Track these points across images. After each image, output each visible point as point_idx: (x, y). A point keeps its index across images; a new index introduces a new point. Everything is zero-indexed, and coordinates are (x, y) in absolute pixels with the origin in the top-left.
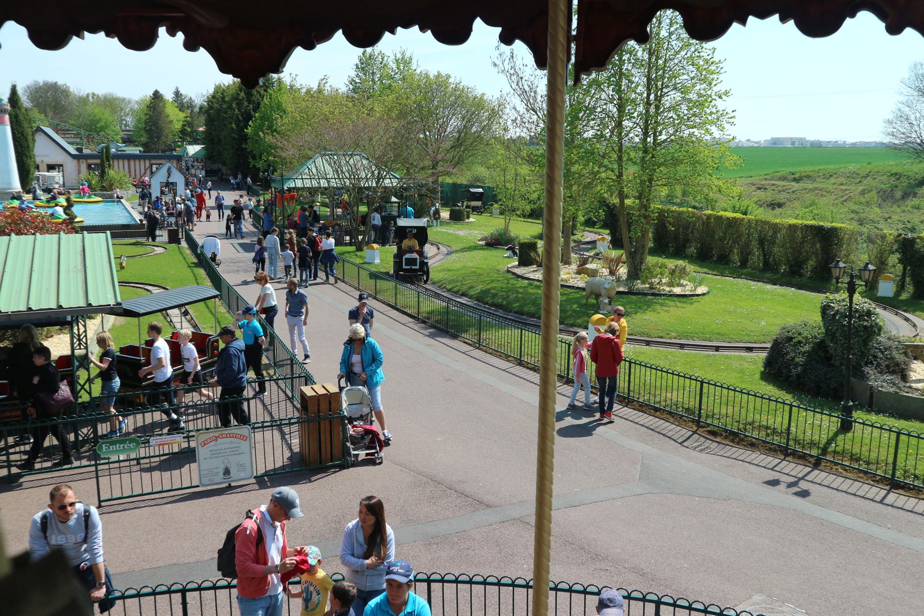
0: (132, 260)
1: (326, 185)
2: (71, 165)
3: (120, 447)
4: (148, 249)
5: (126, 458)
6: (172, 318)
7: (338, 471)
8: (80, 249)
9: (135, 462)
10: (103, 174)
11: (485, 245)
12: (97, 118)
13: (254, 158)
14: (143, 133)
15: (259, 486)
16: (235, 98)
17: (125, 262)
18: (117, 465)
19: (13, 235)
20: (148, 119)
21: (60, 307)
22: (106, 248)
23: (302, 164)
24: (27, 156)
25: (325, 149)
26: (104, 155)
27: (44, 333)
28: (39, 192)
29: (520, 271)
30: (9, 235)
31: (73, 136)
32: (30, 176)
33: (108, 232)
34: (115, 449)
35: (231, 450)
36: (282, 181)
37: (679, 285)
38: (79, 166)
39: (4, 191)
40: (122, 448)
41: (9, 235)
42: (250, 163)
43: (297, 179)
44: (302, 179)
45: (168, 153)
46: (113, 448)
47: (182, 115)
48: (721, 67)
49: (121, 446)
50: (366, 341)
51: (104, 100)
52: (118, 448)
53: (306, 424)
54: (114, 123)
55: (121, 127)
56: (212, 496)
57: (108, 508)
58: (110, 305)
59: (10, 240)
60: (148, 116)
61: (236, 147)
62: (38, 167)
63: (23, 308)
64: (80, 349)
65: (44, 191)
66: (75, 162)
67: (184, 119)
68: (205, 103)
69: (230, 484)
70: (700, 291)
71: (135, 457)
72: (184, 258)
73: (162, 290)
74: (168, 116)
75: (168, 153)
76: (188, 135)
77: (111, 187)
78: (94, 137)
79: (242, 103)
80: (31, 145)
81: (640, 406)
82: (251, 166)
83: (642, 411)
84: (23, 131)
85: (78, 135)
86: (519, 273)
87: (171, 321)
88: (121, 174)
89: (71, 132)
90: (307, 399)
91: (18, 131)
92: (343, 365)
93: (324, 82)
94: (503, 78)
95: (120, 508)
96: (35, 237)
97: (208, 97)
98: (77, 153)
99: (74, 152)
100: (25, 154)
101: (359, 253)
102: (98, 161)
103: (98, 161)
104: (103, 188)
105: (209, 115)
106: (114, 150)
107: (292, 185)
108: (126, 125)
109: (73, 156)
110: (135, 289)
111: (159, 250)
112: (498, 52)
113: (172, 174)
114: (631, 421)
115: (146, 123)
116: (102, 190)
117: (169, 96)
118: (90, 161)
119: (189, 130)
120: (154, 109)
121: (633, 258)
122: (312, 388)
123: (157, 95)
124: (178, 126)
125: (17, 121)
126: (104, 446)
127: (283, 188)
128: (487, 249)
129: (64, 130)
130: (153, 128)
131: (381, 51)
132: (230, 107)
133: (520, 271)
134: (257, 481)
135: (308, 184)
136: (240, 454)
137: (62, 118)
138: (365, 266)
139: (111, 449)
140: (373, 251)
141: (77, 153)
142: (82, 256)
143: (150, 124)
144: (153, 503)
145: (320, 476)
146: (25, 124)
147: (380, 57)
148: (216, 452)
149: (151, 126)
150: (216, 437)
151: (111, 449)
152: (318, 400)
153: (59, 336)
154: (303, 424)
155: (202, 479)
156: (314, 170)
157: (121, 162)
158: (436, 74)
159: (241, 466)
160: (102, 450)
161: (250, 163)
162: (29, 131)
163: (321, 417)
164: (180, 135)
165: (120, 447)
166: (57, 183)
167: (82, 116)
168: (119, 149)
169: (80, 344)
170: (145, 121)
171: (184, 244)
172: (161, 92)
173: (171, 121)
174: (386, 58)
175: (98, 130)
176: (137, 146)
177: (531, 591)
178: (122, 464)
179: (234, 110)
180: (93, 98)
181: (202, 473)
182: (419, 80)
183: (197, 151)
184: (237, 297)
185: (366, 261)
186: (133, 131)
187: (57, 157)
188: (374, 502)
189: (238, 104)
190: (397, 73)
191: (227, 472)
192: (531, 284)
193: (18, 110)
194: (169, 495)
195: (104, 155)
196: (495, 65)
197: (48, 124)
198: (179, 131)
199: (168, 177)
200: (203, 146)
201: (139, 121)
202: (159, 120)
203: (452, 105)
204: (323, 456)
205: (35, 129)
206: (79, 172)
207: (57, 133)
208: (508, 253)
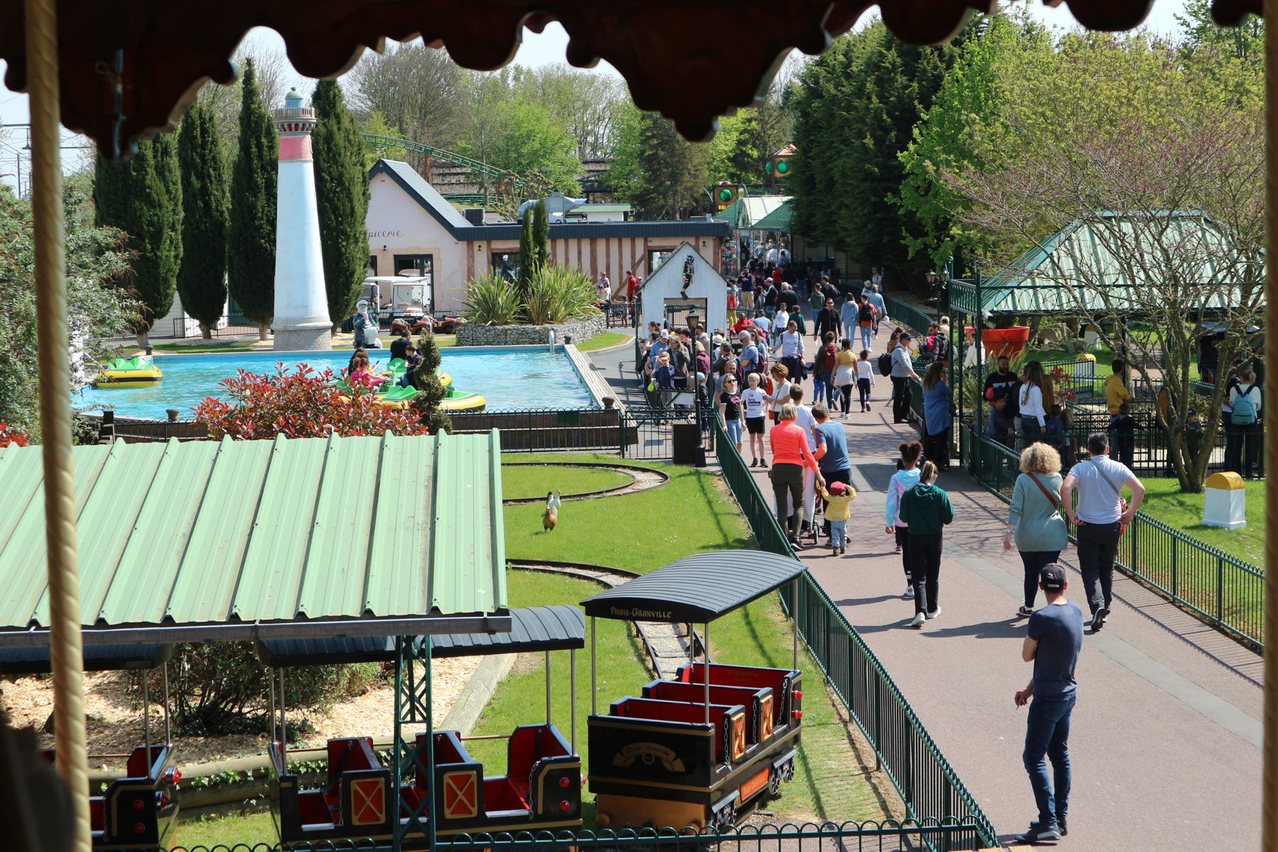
1: (1100, 304)
2: (450, 255)
4: (620, 477)
6: (657, 659)
8: (426, 472)
10: (523, 284)
12: (524, 131)
16: (874, 65)
19: (281, 436)
20: (648, 129)
21: (368, 613)
22: (375, 471)
23: (1036, 248)
24: (348, 238)
26: (531, 230)
27: (344, 682)
30: (219, 438)
31: (462, 179)
32: (354, 286)
33: (496, 432)
38: (471, 257)
39: (290, 326)
41: (219, 438)
43: (1019, 287)
44: (1034, 287)
48: (309, 366)
51: (543, 85)
54: (566, 142)
58: (481, 614)
59: (219, 449)
61: (873, 199)
62: (373, 263)
63: (287, 613)
64: (413, 720)
65: (384, 323)
67: (742, 127)
68: (798, 82)
72: (709, 503)
73: (628, 580)
79: (893, 80)
80: (359, 210)
84: (341, 174)
87: (655, 668)
89: (458, 170)
91: (330, 174)
96: (329, 442)
98: (466, 224)
99: (460, 222)
100: (344, 233)
101: (1189, 499)
102: (515, 245)
103: (515, 245)
104: (524, 316)
105: (805, 115)
107: (1006, 306)
108: (595, 148)
109: (458, 234)
110: (575, 580)
111: (647, 481)
113: (695, 277)
116: (521, 321)
118: (498, 245)
125: (330, 150)
130: (662, 153)
132: (860, 92)
135: (1049, 301)
138: (1196, 536)
140: (1224, 492)
141: (466, 224)
146: (348, 158)
149: (656, 147)
153: (381, 693)
156: (1067, 264)
157: (573, 244)
162: (356, 173)
164: (732, 170)
166: (416, 303)
169: (412, 711)
170: (641, 134)
176: (618, 200)
179: (869, 98)
180: (516, 79)
183: (770, 210)
185: (1206, 520)
187: (421, 237)
189: (880, 82)
193: (333, 122)
195: (531, 230)
197: (404, 152)
198: (729, 158)
199: (686, 286)
206: (470, 273)
207: (425, 175)
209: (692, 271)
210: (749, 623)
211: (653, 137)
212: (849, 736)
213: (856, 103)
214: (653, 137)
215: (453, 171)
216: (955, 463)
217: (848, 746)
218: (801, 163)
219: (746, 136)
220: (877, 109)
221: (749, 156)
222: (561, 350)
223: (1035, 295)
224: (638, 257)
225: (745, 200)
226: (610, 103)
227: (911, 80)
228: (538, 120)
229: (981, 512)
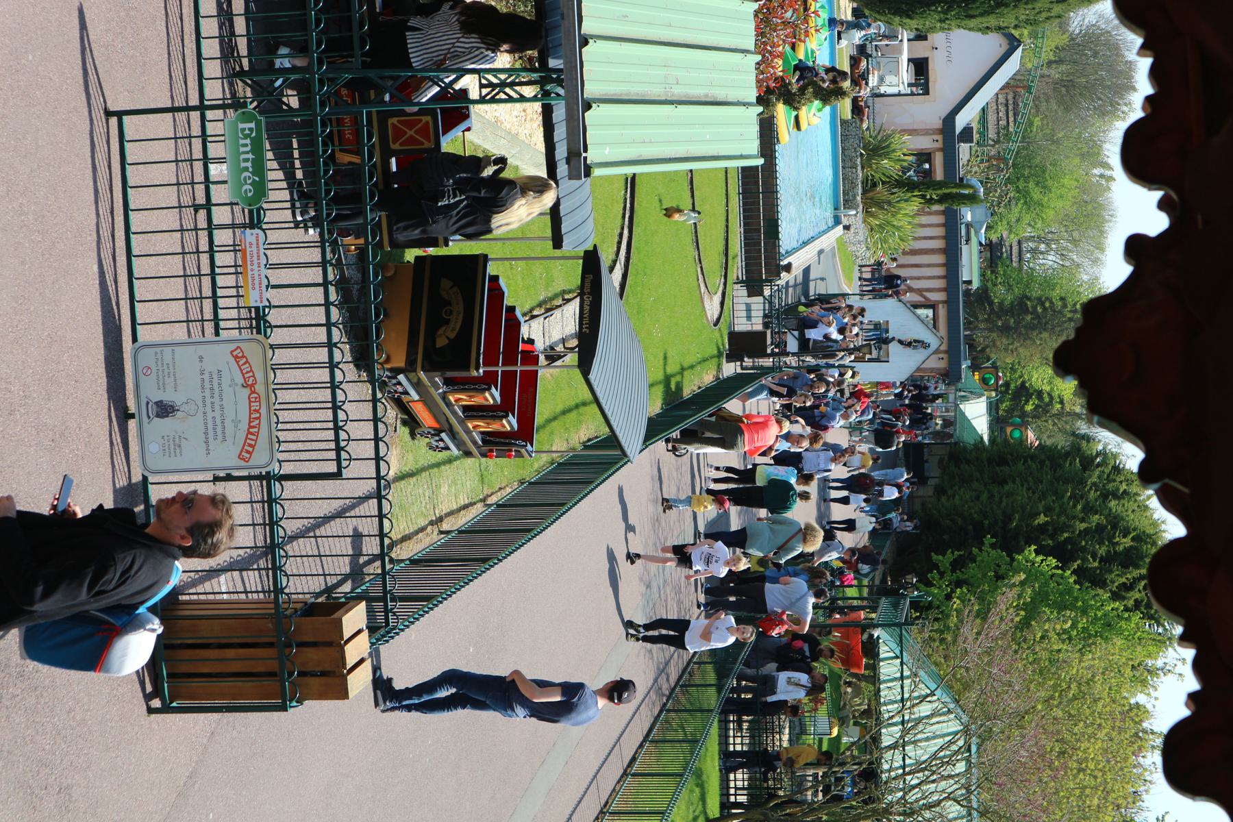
0: (688, 239)
1: (886, 741)
2: (929, 112)
3: (246, 160)
4: (716, 281)
6: (541, 319)
7: (143, 689)
8: (721, 95)
13: (957, 565)
15: (121, 489)
17: (683, 218)
21: (585, 42)
23: (940, 679)
24: (945, 13)
25: (983, 741)
28: (857, 36)
31: (1003, 123)
32: (897, 19)
33: (760, 162)
34: (242, 149)
35: (218, 422)
36: (895, 625)
38: (926, 132)
40: (243, 165)
42: (944, 555)
43: (902, 663)
44: (902, 678)
45: (964, 348)
46: (246, 145)
49: (249, 164)
53: (273, 611)
55: (1031, 238)
56: (107, 372)
57: (103, 131)
58: (586, 150)
61: (987, 522)
62: (920, 37)
66: (938, 124)
68: (1100, 447)
69: (132, 416)
75: (964, 348)
77: (872, 204)
78: (999, 170)
79: (1101, 543)
80: (972, 23)
82: (934, 556)
85: (1004, 135)
87: (533, 317)
89: (1011, 119)
90: (336, 615)
95: (101, 157)
97: (1115, 456)
98: (958, 129)
99: (961, 121)
102: (939, 175)
103: (939, 175)
104: (870, 185)
106: (969, 217)
107: (884, 652)
108: (1034, 251)
109: (949, 120)
110: (616, 239)
111: (712, 307)
113: (909, 351)
115: (1041, 301)
116: (865, 182)
118: (938, 159)
119: (1029, 408)
122: (359, 632)
126: (252, 125)
129: (1016, 104)
132: (1089, 509)
134: (136, 484)
135: (889, 692)
136: (207, 442)
137: (1047, 101)
139: (242, 142)
141: (958, 129)
142: (703, 99)
144: (105, 233)
148: (216, 386)
149: (1034, 312)
150: (252, 385)
151: (242, 142)
152: (329, 644)
155: (152, 350)
157: (940, 231)
159: (175, 445)
161: (944, 555)
162: (1008, 19)
163: (287, 651)
164: (1012, 386)
165: (246, 160)
166: (881, 79)
167: (1054, 148)
168: (972, 231)
171: (730, 369)
175: (1021, 184)
176: (983, 275)
177: (236, 208)
179: (1083, 520)
180: (1102, 176)
181: (168, 350)
183: (974, 423)
186: (1020, 269)
189: (1100, 528)
191: (164, 410)
194: (119, 271)
195: (954, 191)
197: (1029, 66)
198: (1023, 383)
199: (900, 342)
200: (986, 438)
201: (1048, 283)
205: (1016, 33)
209: (915, 348)
211: (1045, 309)
212: (472, 504)
214: (1045, 309)
215: (1011, 114)
219: (1047, 400)
221: (1027, 402)
222: (837, 221)
223: (895, 679)
225: (984, 398)
228: (1061, 197)
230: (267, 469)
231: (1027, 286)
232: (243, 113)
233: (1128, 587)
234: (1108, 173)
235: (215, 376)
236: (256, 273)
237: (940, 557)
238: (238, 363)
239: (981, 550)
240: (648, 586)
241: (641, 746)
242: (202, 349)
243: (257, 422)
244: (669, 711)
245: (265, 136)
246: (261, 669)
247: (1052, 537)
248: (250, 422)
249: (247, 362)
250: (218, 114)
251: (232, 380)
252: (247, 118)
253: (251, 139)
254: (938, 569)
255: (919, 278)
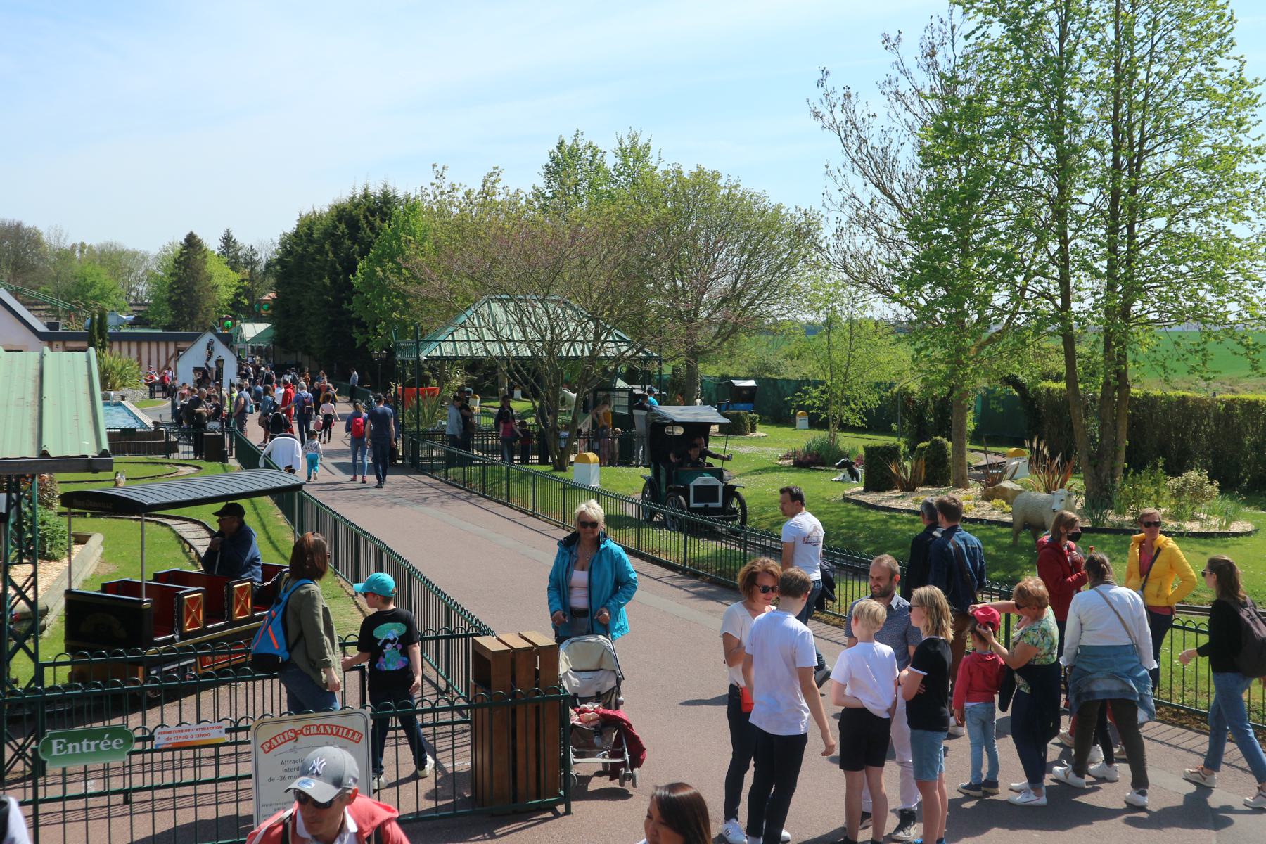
3: (89, 746)
4: (168, 469)
5: (102, 790)
9: (120, 798)
11: (793, 466)
12: (89, 281)
14: (166, 307)
18: (80, 803)
20: (174, 283)
29: (871, 498)
34: (78, 751)
36: (418, 345)
37: (1193, 518)
40: (93, 749)
43: (444, 341)
44: (454, 341)
46: (74, 747)
47: (234, 277)
49: (93, 743)
50: (602, 546)
51: (100, 256)
52: (85, 750)
53: (486, 710)
58: (86, 456)
60: (174, 279)
70: (1237, 527)
71: (120, 786)
74: (210, 278)
76: (244, 308)
79: (342, 243)
81: (1175, 715)
83: (1182, 726)
85: (55, 310)
86: (870, 502)
88: (125, 359)
89: (40, 307)
92: (555, 593)
93: (493, 178)
94: (833, 142)
98: (46, 330)
99: (41, 328)
109: (41, 336)
112: (822, 90)
114: (1162, 743)
115: (172, 290)
117: (213, 244)
120: (187, 266)
121: (1095, 466)
123: (192, 242)
124: (226, 295)
126: (55, 742)
127: (418, 358)
128: (793, 471)
130: (184, 299)
131: (591, 143)
132: (321, 250)
133: (871, 498)
139: (70, 751)
141: (46, 330)
143: (179, 291)
145: (513, 826)
147: (589, 153)
151: (70, 751)
152: (513, 662)
154: (479, 711)
158: (695, 170)
160: (51, 751)
165: (89, 746)
167: (62, 276)
170: (171, 285)
172: (200, 235)
173: (216, 287)
174: (599, 155)
178: (92, 802)
179: (327, 255)
180: (81, 251)
182: (666, 183)
183: (259, 332)
184: (336, 521)
188: (681, 798)
189: (334, 245)
190: (621, 174)
192: (891, 517)
196: (817, 114)
198: (229, 305)
202: (194, 284)
203: (722, 226)
204: (521, 786)
208: (844, 473)
209: (213, 349)
210: (272, 542)
211: (178, 288)
212: (357, 604)
213: (318, 257)
214: (178, 288)
215: (36, 307)
216: (399, 462)
217: (356, 610)
218: (277, 304)
219: (241, 290)
220: (332, 261)
221: (243, 303)
222: (118, 404)
223: (455, 345)
224: (170, 354)
225: (242, 325)
226: (147, 270)
227: (354, 244)
228: (98, 275)
229: (420, 484)
230: (369, 717)
231: (162, 300)
232: (42, 751)
233: (373, 228)
234: (78, 247)
235: (287, 766)
236: (195, 733)
237: (357, 342)
238: (275, 747)
239: (353, 312)
240: (395, 503)
241: (511, 507)
242: (263, 780)
243: (328, 728)
244: (484, 492)
245: (70, 730)
246: (532, 720)
247: (338, 275)
248: (327, 734)
249: (275, 738)
250: (41, 790)
251: (290, 750)
252: (48, 746)
253: (68, 743)
254: (366, 343)
255: (158, 361)
